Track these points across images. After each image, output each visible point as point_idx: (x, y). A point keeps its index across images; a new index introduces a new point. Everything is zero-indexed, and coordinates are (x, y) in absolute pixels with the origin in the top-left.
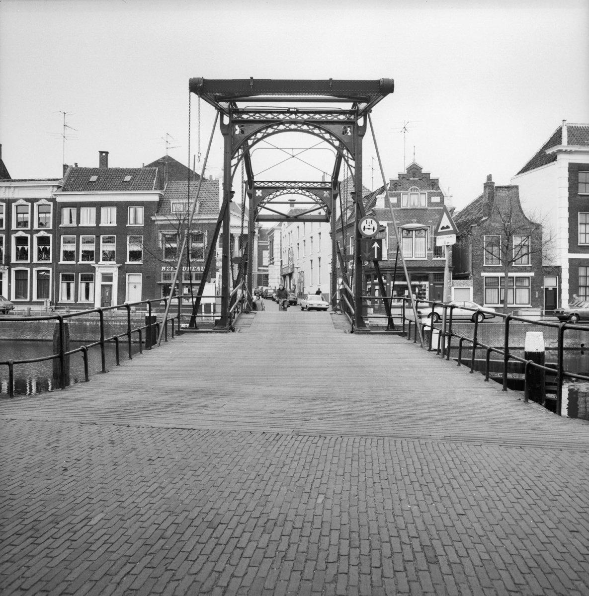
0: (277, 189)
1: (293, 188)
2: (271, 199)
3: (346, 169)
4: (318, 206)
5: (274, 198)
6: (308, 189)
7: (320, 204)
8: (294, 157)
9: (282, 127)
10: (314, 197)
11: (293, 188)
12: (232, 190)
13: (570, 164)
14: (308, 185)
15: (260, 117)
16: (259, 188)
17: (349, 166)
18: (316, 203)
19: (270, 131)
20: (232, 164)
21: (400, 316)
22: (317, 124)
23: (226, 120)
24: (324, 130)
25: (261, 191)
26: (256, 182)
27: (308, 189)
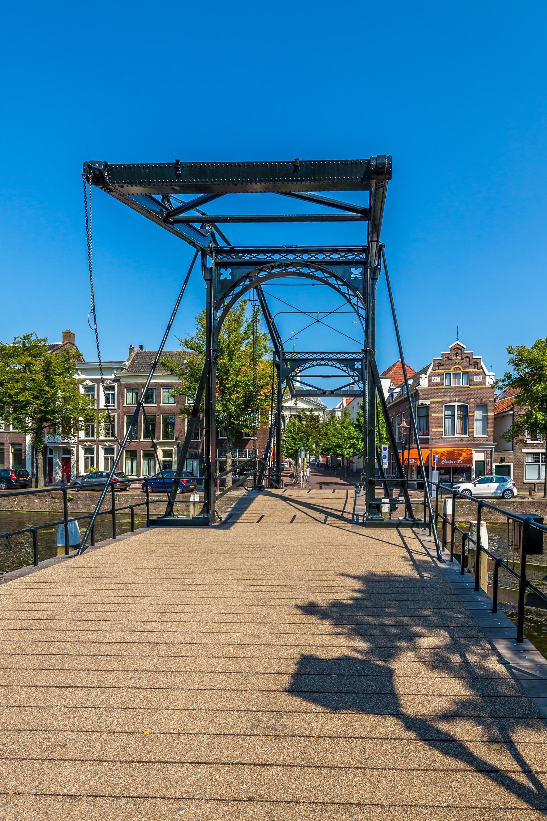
0: (307, 360)
1: (322, 359)
6: (339, 360)
8: (318, 321)
9: (315, 363)
10: (345, 369)
11: (322, 359)
13: (541, 553)
14: (339, 356)
15: (251, 258)
21: (136, 516)
22: (320, 265)
23: (210, 263)
24: (328, 272)
27: (339, 360)
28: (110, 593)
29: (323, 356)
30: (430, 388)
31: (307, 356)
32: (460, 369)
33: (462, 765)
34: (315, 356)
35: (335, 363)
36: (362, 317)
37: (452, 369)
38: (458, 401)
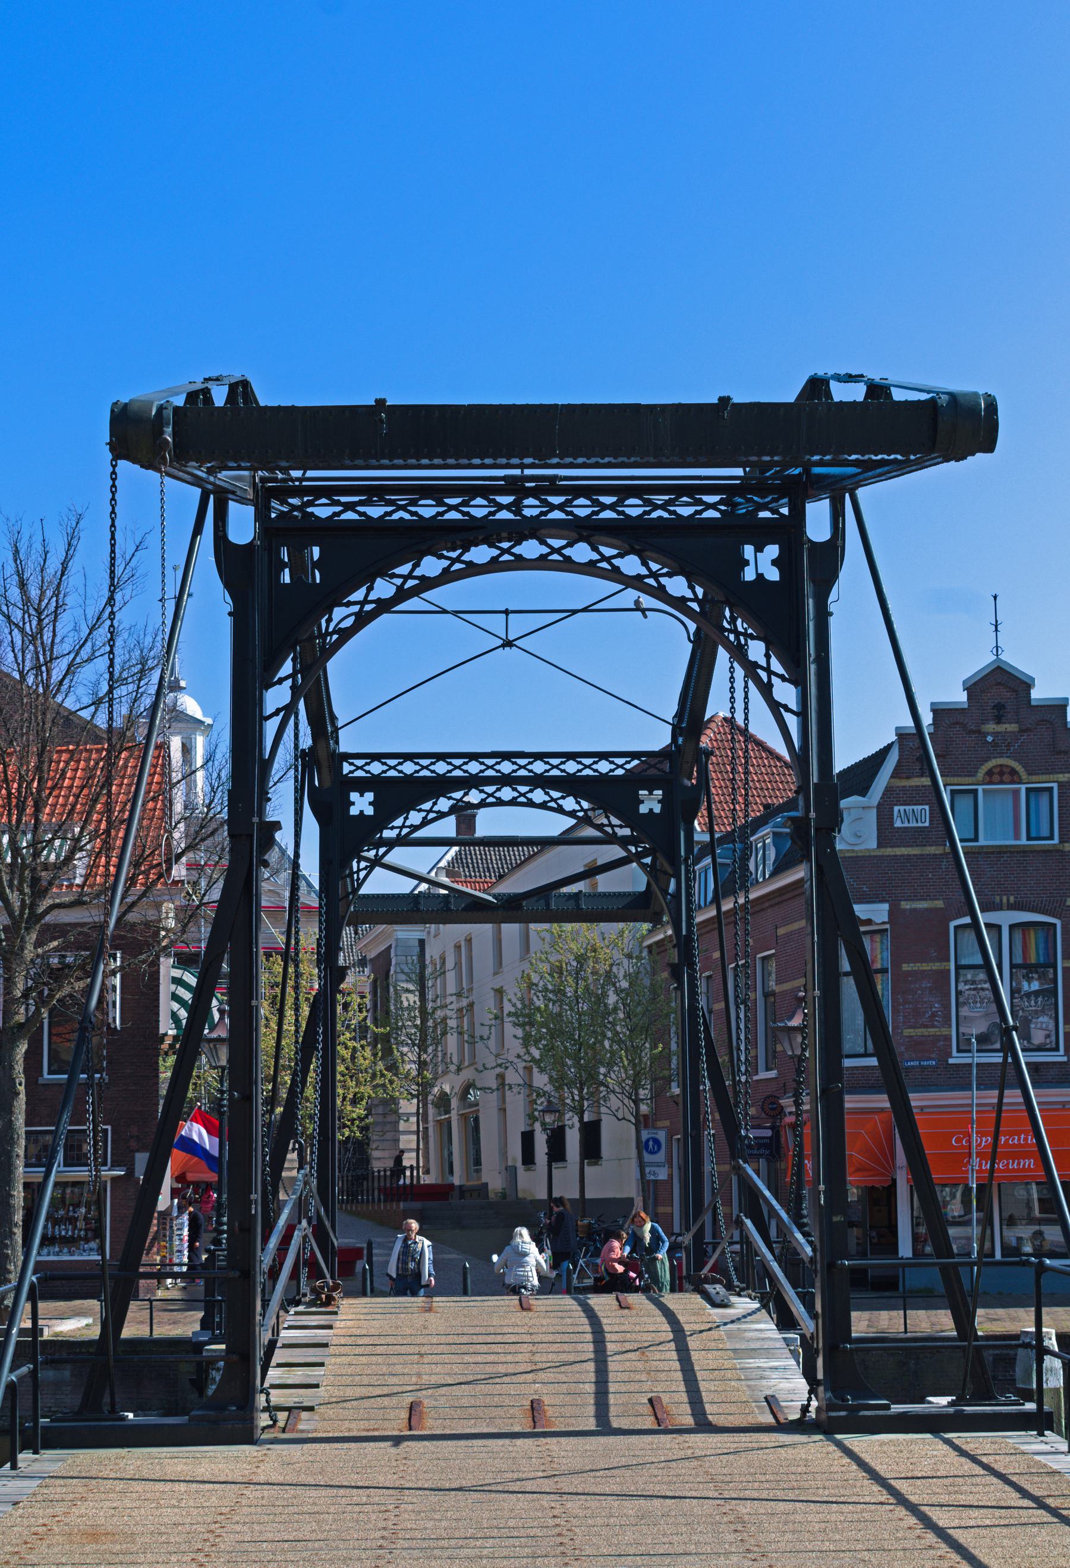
2: (415, 828)
3: (739, 684)
4: (616, 852)
5: (425, 823)
6: (570, 785)
7: (623, 842)
8: (508, 644)
9: (481, 554)
12: (270, 818)
16: (362, 785)
17: (751, 668)
18: (611, 839)
19: (431, 566)
20: (269, 710)
25: (370, 796)
26: (347, 757)
27: (570, 785)
28: (423, 1350)
29: (506, 767)
30: (889, 851)
31: (441, 768)
32: (1013, 772)
33: (1056, 1520)
34: (474, 767)
35: (555, 794)
36: (787, 709)
37: (981, 774)
38: (1012, 907)
